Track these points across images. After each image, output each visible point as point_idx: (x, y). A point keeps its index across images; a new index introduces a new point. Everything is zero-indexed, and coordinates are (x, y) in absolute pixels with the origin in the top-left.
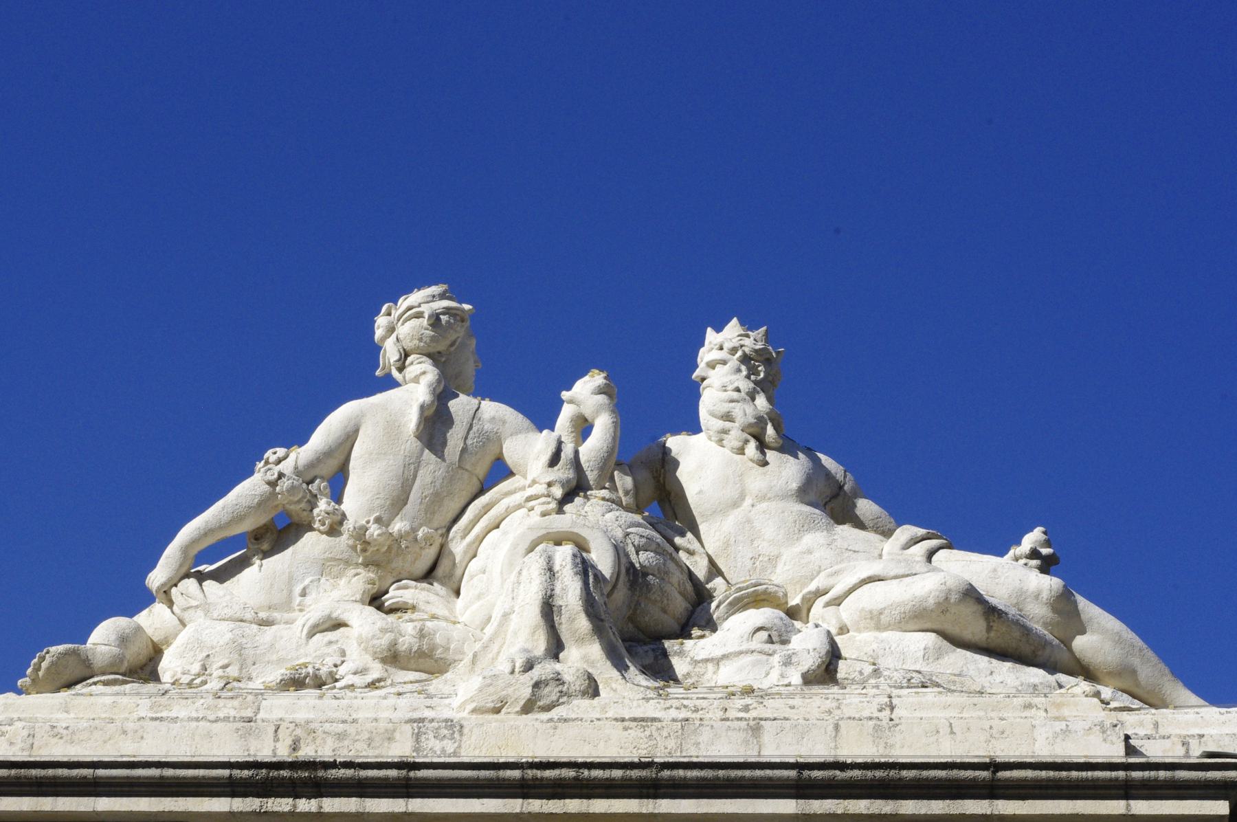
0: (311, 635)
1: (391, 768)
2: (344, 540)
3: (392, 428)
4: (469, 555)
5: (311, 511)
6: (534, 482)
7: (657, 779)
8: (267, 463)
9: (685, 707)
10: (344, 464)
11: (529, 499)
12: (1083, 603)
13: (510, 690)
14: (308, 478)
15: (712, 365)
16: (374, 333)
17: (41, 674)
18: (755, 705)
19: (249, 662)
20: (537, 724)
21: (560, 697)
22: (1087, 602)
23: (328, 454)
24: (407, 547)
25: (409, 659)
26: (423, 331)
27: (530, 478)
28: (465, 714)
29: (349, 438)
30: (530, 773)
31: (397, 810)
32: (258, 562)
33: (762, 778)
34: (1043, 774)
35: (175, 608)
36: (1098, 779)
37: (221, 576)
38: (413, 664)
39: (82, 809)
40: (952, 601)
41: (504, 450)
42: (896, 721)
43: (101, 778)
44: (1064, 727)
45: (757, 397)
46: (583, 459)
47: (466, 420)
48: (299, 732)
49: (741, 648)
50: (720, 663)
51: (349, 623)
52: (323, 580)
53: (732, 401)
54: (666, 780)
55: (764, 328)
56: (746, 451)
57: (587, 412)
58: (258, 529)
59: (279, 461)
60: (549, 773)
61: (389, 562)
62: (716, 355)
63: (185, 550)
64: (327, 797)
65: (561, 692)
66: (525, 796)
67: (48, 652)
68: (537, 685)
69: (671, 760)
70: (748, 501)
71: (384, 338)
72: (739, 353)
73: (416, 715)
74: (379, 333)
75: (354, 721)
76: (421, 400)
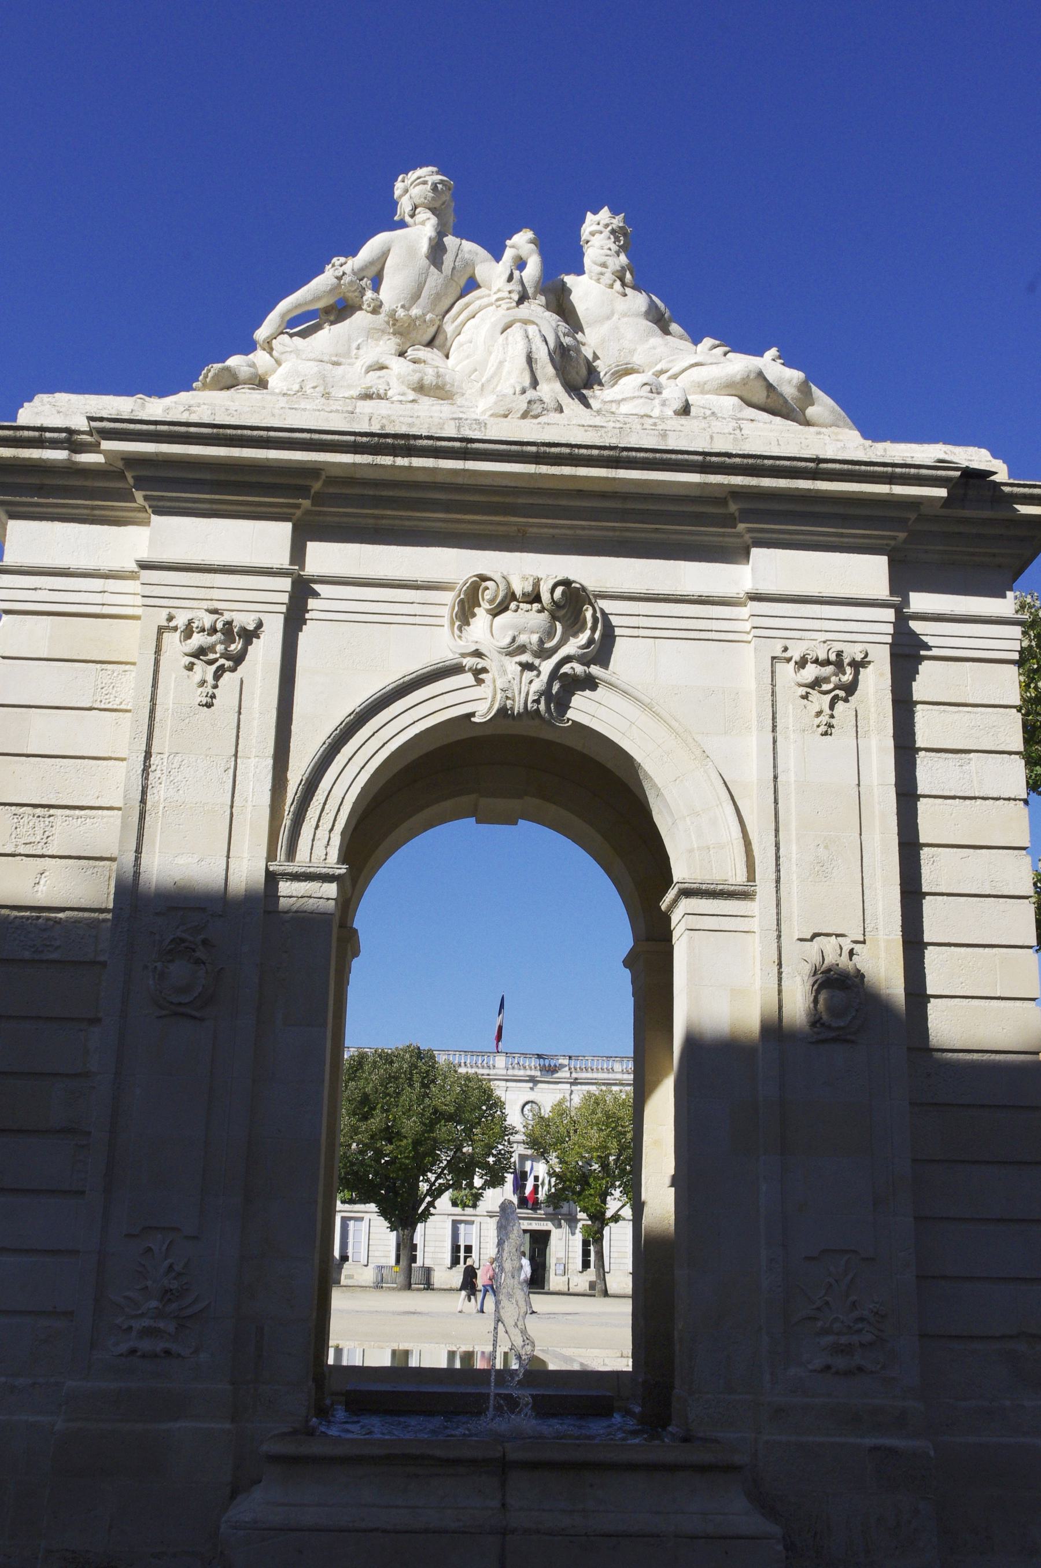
0: (367, 372)
1: (456, 441)
2: (382, 317)
3: (411, 251)
4: (457, 333)
5: (362, 297)
6: (499, 290)
7: (619, 457)
8: (333, 266)
9: (618, 421)
10: (380, 272)
11: (498, 300)
12: (814, 388)
13: (514, 405)
14: (360, 277)
15: (593, 234)
16: (394, 193)
17: (208, 380)
18: (660, 423)
19: (329, 386)
20: (532, 425)
21: (543, 411)
22: (817, 388)
23: (372, 263)
24: (420, 325)
25: (431, 389)
26: (427, 193)
27: (494, 289)
28: (486, 417)
29: (384, 255)
30: (542, 449)
31: (458, 467)
32: (328, 327)
33: (682, 460)
34: (846, 467)
35: (274, 353)
36: (876, 472)
37: (304, 334)
38: (432, 393)
39: (259, 456)
40: (751, 377)
41: (476, 272)
42: (745, 436)
43: (272, 437)
44: (843, 445)
45: (621, 255)
46: (525, 280)
47: (455, 250)
48: (384, 421)
49: (635, 395)
50: (621, 404)
51: (390, 366)
52: (369, 341)
53: (607, 256)
54: (625, 458)
55: (623, 214)
56: (614, 286)
57: (523, 253)
58: (327, 307)
59: (341, 265)
60: (553, 450)
61: (409, 333)
62: (595, 228)
63: (283, 316)
64: (414, 457)
65: (543, 408)
66: (537, 463)
67: (212, 367)
68: (529, 402)
69: (629, 446)
70: (616, 317)
71: (401, 196)
72: (610, 228)
73: (455, 416)
74: (397, 193)
75: (418, 417)
76: (429, 234)
